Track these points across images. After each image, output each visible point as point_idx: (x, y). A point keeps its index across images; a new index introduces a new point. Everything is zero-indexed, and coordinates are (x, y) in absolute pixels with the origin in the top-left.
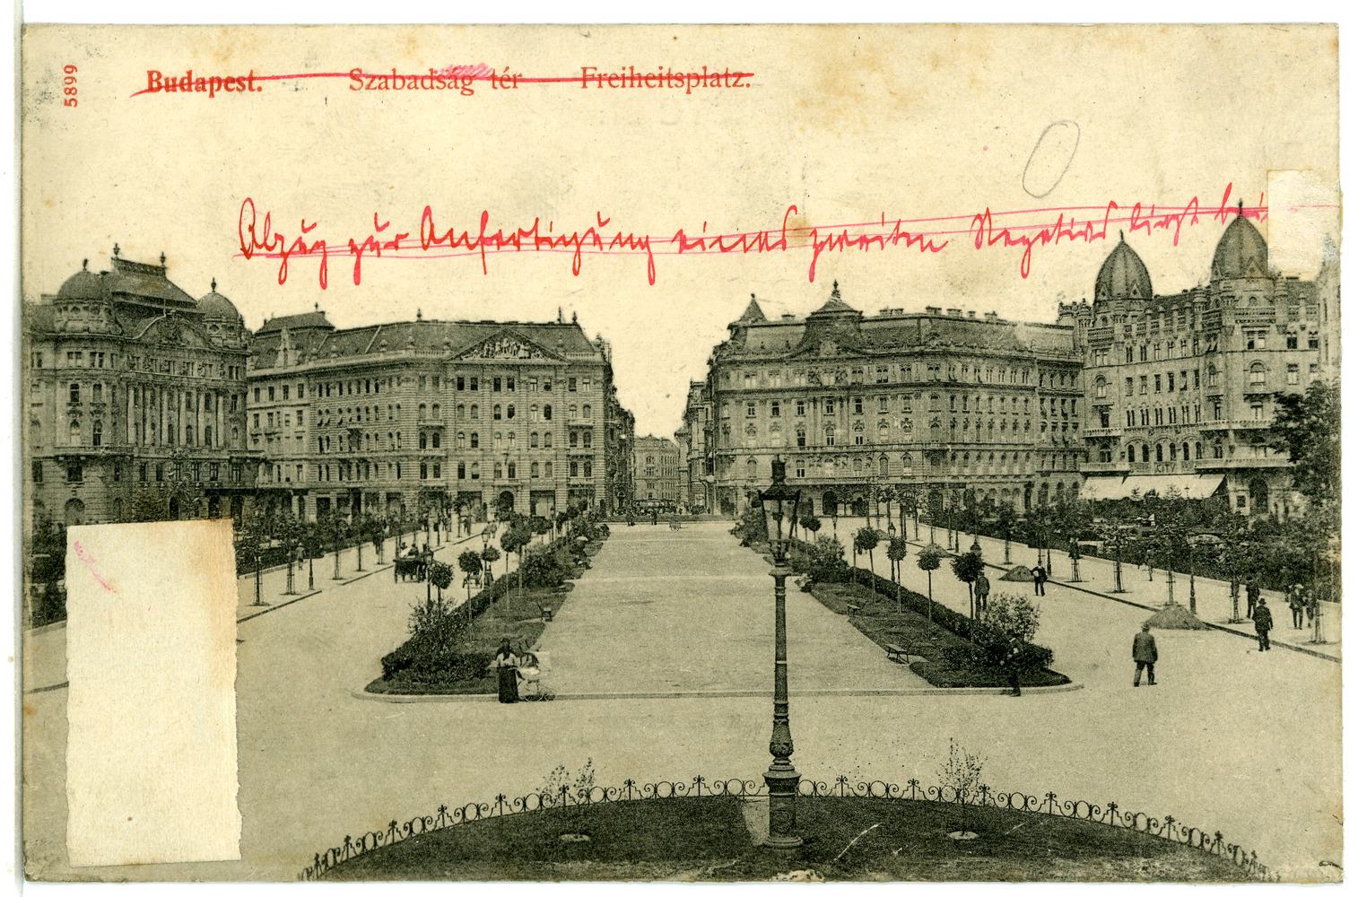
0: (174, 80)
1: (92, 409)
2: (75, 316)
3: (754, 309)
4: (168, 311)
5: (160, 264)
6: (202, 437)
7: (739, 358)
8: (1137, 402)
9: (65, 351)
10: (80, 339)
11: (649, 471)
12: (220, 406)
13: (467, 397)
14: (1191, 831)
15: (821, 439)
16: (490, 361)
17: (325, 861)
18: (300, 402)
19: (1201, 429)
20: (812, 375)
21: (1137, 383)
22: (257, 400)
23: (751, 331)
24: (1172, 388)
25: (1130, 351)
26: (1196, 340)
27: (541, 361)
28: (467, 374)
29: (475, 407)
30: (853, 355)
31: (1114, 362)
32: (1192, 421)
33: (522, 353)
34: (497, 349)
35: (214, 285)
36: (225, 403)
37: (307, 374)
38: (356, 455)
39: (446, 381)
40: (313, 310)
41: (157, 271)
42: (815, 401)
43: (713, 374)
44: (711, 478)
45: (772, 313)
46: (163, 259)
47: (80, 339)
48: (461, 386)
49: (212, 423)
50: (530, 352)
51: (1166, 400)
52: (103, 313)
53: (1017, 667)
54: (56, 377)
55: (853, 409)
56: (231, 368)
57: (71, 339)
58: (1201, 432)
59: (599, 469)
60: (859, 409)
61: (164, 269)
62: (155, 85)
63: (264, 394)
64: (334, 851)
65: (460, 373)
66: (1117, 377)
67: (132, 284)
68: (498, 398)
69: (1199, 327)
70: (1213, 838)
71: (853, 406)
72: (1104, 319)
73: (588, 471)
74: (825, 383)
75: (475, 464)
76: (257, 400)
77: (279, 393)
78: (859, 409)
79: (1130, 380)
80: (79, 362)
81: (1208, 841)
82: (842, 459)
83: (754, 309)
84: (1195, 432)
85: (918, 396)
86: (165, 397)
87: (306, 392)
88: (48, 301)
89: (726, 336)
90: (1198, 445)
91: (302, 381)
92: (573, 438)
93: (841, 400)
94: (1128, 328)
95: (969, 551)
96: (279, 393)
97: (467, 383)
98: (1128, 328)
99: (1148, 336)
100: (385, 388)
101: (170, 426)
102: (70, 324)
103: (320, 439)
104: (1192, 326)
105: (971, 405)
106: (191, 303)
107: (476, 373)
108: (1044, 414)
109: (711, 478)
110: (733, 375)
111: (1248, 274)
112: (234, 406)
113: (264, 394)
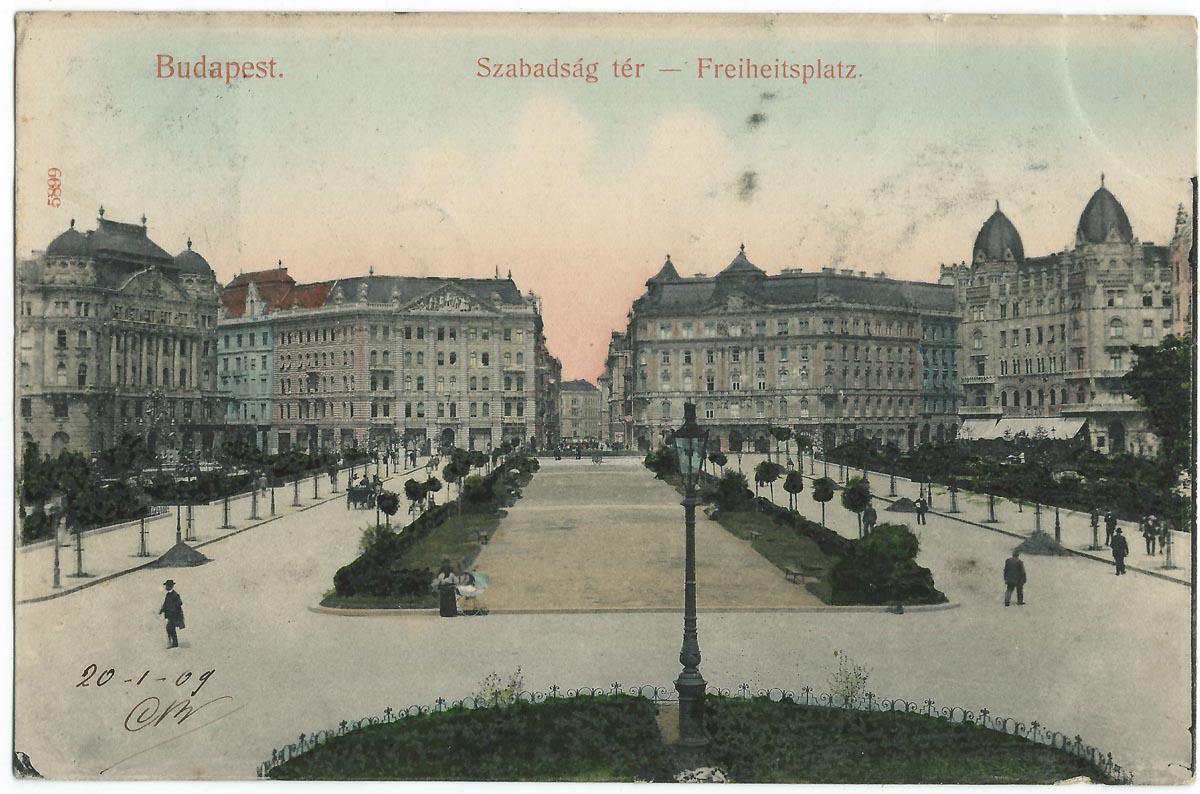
1: (78, 353)
2: (63, 270)
3: (669, 268)
13: (415, 345)
14: (1054, 735)
17: (282, 757)
19: (1066, 377)
20: (721, 328)
22: (227, 346)
24: (1040, 341)
33: (462, 306)
34: (441, 302)
35: (190, 244)
36: (198, 348)
37: (273, 323)
39: (395, 331)
40: (277, 267)
42: (723, 350)
46: (144, 220)
55: (757, 358)
56: (204, 317)
58: (1068, 381)
63: (233, 341)
64: (290, 747)
67: (117, 241)
73: (520, 411)
75: (421, 404)
76: (227, 346)
80: (66, 311)
83: (669, 268)
86: (161, 343)
92: (508, 381)
96: (246, 340)
102: (58, 277)
111: (1108, 239)
113: (233, 341)
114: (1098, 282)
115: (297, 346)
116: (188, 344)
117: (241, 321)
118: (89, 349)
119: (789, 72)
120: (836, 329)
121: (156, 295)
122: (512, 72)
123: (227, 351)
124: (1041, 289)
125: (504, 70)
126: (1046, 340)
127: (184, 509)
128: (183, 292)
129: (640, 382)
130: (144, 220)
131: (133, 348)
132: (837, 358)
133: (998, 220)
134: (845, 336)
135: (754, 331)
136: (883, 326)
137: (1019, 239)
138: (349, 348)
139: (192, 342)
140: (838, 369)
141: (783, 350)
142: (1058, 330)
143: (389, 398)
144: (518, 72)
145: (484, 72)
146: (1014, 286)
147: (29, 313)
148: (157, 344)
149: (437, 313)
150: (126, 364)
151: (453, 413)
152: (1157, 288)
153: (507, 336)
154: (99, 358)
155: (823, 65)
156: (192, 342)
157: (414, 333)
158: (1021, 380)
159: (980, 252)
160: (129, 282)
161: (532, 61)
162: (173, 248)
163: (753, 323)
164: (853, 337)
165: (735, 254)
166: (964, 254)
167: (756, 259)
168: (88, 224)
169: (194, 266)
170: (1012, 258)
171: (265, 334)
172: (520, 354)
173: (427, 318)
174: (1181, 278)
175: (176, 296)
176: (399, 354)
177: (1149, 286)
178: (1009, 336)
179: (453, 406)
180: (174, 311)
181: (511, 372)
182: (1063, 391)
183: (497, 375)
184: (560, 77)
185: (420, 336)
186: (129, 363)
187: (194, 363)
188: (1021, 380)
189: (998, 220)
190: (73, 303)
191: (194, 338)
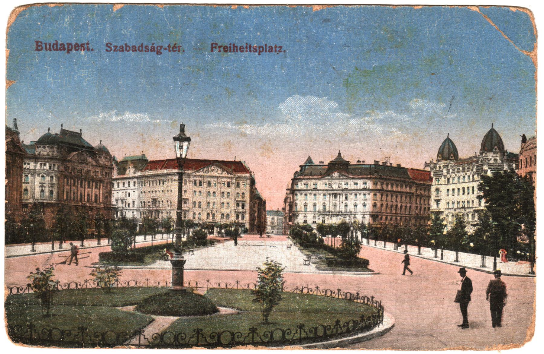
1: (44, 185)
2: (44, 150)
3: (309, 160)
6: (93, 198)
10: (45, 159)
11: (272, 223)
12: (101, 187)
13: (197, 189)
15: (332, 209)
19: (474, 209)
20: (330, 185)
21: (451, 192)
22: (118, 187)
26: (473, 176)
27: (227, 175)
30: (344, 177)
31: (443, 183)
32: (471, 206)
33: (219, 172)
34: (210, 170)
35: (49, 130)
36: (103, 186)
37: (138, 177)
39: (190, 181)
42: (330, 194)
43: (293, 184)
45: (316, 162)
46: (81, 130)
47: (45, 159)
48: (195, 184)
51: (465, 198)
52: (55, 149)
53: (270, 288)
54: (35, 173)
55: (344, 198)
56: (106, 173)
57: (42, 158)
58: (474, 210)
59: (247, 216)
60: (346, 198)
61: (81, 134)
63: (121, 185)
65: (195, 178)
66: (443, 189)
67: (68, 139)
69: (475, 170)
72: (440, 167)
73: (243, 218)
74: (334, 188)
75: (200, 214)
76: (118, 187)
77: (126, 185)
78: (346, 198)
79: (448, 190)
80: (45, 168)
83: (309, 160)
84: (472, 210)
85: (369, 194)
86: (87, 183)
87: (136, 184)
88: (34, 143)
89: (299, 169)
91: (136, 180)
92: (238, 205)
93: (340, 194)
94: (448, 170)
95: (421, 167)
96: (126, 185)
97: (198, 183)
98: (448, 170)
99: (456, 173)
100: (166, 183)
102: (42, 153)
103: (141, 202)
104: (472, 170)
106: (93, 148)
108: (416, 204)
109: (290, 223)
110: (299, 184)
111: (494, 150)
113: (121, 185)
114: (489, 168)
115: (149, 187)
116: (84, 182)
117: (125, 176)
118: (54, 184)
119: (252, 49)
120: (379, 187)
121: (84, 162)
122: (122, 49)
123: (124, 188)
125: (118, 48)
126: (466, 193)
128: (97, 161)
129: (295, 207)
130: (81, 130)
131: (74, 183)
132: (379, 199)
135: (344, 187)
137: (457, 152)
139: (93, 182)
140: (379, 205)
142: (471, 189)
144: (124, 49)
145: (109, 49)
146: (454, 170)
147: (442, 258)
148: (100, 186)
150: (77, 192)
151: (213, 218)
152: (456, 175)
154: (59, 188)
156: (93, 182)
157: (198, 183)
158: (455, 210)
159: (440, 155)
160: (74, 155)
162: (95, 144)
163: (343, 183)
164: (386, 191)
165: (336, 156)
166: (434, 156)
168: (56, 130)
169: (103, 151)
170: (453, 158)
171: (134, 182)
172: (243, 193)
173: (204, 177)
175: (94, 163)
177: (448, 176)
178: (451, 192)
181: (239, 201)
182: (472, 215)
184: (144, 52)
185: (200, 185)
186: (65, 190)
187: (101, 192)
188: (455, 210)
190: (48, 165)
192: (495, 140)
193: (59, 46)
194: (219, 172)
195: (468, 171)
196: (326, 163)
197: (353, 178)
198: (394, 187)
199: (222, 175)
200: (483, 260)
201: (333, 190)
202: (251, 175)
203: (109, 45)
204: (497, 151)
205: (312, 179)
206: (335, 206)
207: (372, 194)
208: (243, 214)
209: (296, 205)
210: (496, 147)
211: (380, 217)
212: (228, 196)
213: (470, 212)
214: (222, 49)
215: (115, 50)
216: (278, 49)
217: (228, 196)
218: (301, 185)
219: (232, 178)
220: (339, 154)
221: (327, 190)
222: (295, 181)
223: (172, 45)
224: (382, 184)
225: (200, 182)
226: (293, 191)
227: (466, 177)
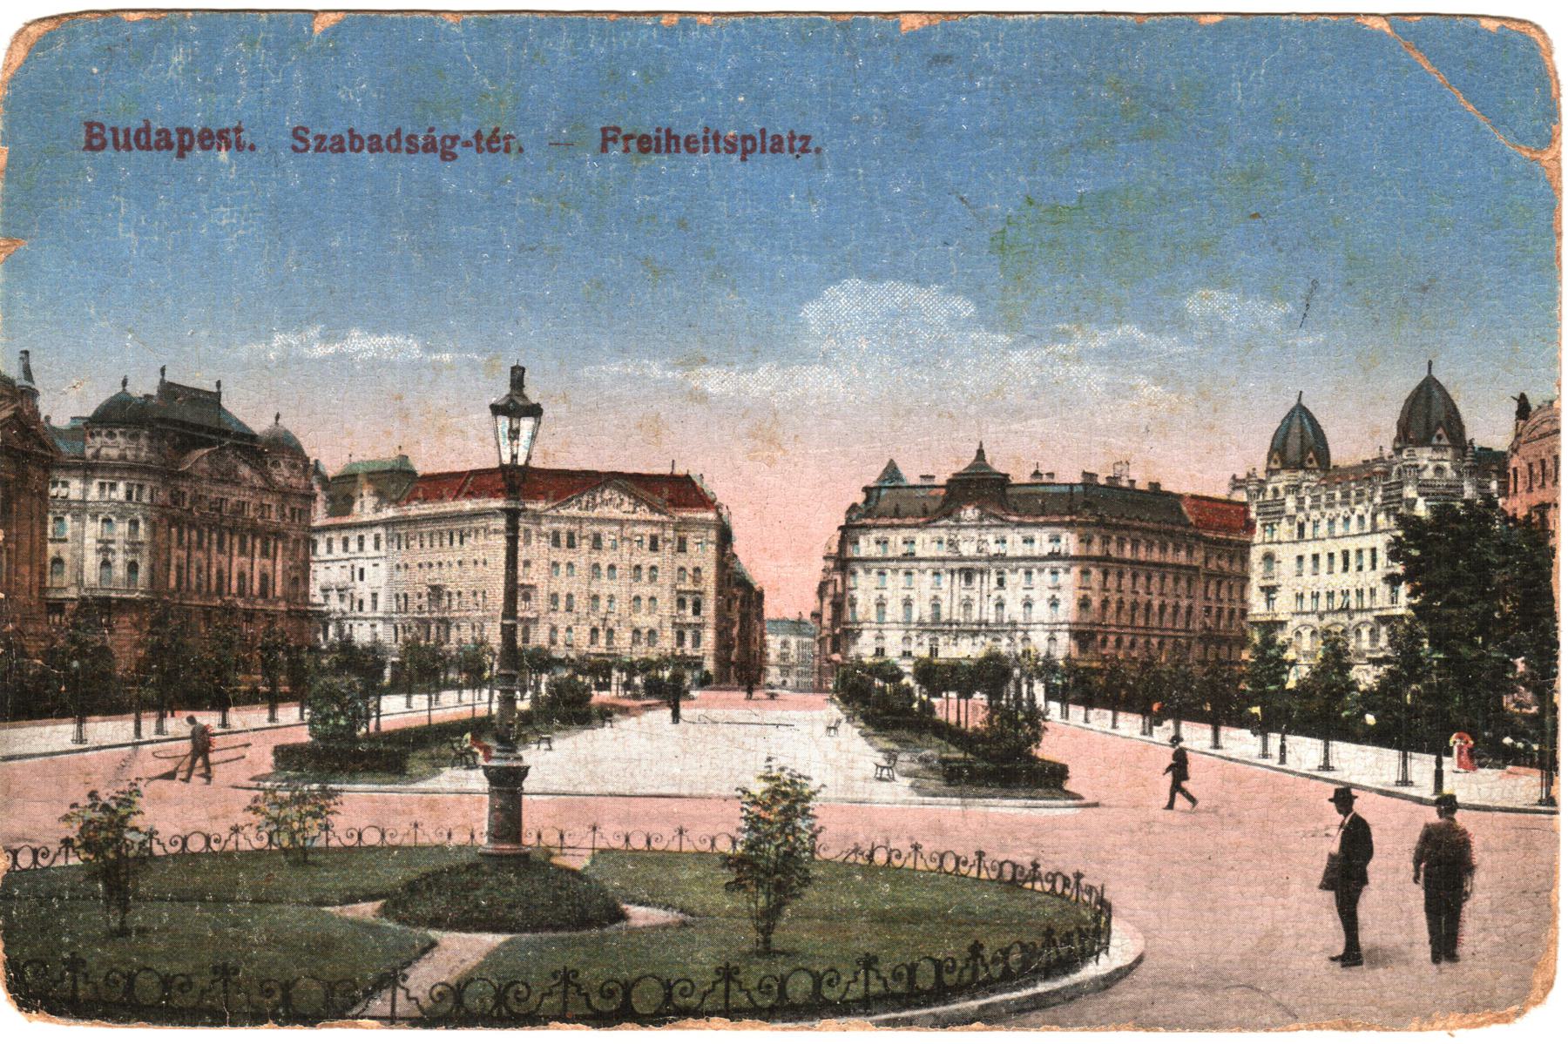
0: (127, 132)
1: (112, 546)
2: (110, 442)
3: (892, 472)
4: (221, 442)
5: (215, 390)
6: (256, 586)
7: (869, 521)
8: (1308, 582)
9: (96, 482)
10: (115, 469)
12: (280, 552)
13: (563, 556)
16: (589, 514)
18: (376, 553)
19: (1377, 613)
20: (952, 543)
21: (1324, 560)
22: (330, 551)
23: (884, 492)
24: (1374, 567)
25: (1301, 527)
26: (1374, 516)
28: (563, 527)
29: (653, 568)
30: (995, 522)
32: (1367, 605)
33: (626, 507)
34: (598, 500)
35: (124, 383)
36: (285, 549)
37: (386, 524)
38: (435, 615)
39: (539, 534)
41: (212, 400)
42: (952, 572)
43: (842, 543)
44: (836, 657)
46: (219, 384)
48: (556, 542)
49: (269, 569)
50: (635, 506)
54: (85, 510)
56: (292, 509)
57: (104, 468)
58: (1377, 618)
59: (709, 636)
60: (1001, 582)
61: (219, 394)
62: (96, 142)
63: (337, 546)
65: (555, 525)
66: (1286, 555)
68: (682, 560)
69: (1378, 500)
70: (972, 858)
71: (994, 578)
73: (697, 641)
74: (965, 554)
75: (569, 629)
76: (330, 551)
77: (353, 546)
78: (1001, 582)
79: (1300, 558)
80: (113, 495)
81: (965, 863)
82: (982, 638)
83: (892, 472)
84: (1370, 617)
85: (1067, 571)
86: (236, 540)
87: (383, 544)
88: (80, 423)
89: (860, 498)
90: (1372, 632)
91: (380, 530)
92: (681, 603)
94: (1301, 501)
96: (353, 546)
97: (563, 538)
98: (1301, 501)
99: (1323, 509)
100: (469, 541)
101: (220, 572)
103: (397, 596)
105: (1224, 594)
106: (253, 437)
107: (655, 531)
108: (1207, 599)
109: (836, 657)
110: (862, 540)
111: (1435, 441)
112: (294, 553)
113: (337, 546)
114: (1421, 495)
118: (141, 543)
120: (1096, 550)
122: (338, 146)
124: (1348, 503)
125: (328, 143)
127: (525, 798)
128: (267, 477)
130: (219, 384)
132: (1096, 586)
133: (1300, 412)
134: (1106, 558)
135: (994, 549)
136: (1156, 550)
137: (1326, 446)
138: (479, 555)
140: (1096, 602)
141: (1028, 573)
143: (529, 619)
145: (301, 145)
146: (1316, 499)
149: (594, 515)
153: (682, 547)
155: (153, 132)
157: (563, 538)
158: (1321, 617)
161: (365, 131)
162: (260, 424)
164: (1117, 561)
167: (998, 463)
168: (144, 386)
169: (283, 446)
170: (1315, 464)
171: (377, 538)
173: (581, 520)
174: (1520, 488)
175: (258, 482)
176: (543, 563)
179: (611, 632)
180: (243, 493)
181: (686, 592)
183: (667, 595)
187: (279, 567)
188: (1321, 617)
189: (1300, 412)
190: (121, 486)
191: (279, 535)
192: (1439, 412)
193: (154, 138)
194: (626, 507)
195: (1358, 503)
196: (941, 479)
197: (1020, 525)
198: (1142, 549)
199: (634, 517)
200: (1405, 764)
201: (961, 559)
202: (720, 515)
203: (301, 133)
204: (1445, 442)
205: (899, 526)
206: (967, 605)
207: (1076, 570)
208: (698, 629)
209: (853, 605)
210: (1440, 431)
211: (1099, 637)
212: (653, 579)
213: (1365, 623)
214: (633, 144)
215: (317, 149)
216: (798, 144)
217: (653, 579)
218: (866, 546)
219: (663, 524)
220: (980, 452)
221: (944, 560)
222: (848, 532)
223: (487, 134)
224: (1106, 541)
225: (571, 536)
226: (842, 563)
227: (1354, 519)
